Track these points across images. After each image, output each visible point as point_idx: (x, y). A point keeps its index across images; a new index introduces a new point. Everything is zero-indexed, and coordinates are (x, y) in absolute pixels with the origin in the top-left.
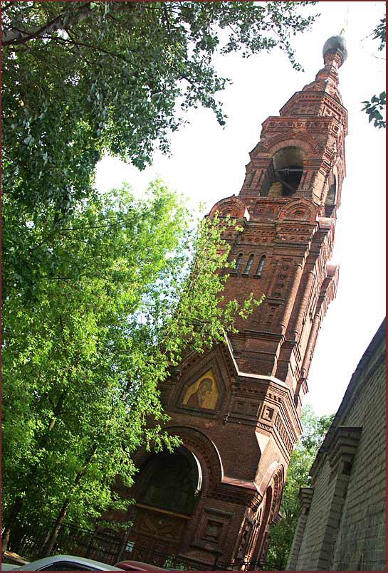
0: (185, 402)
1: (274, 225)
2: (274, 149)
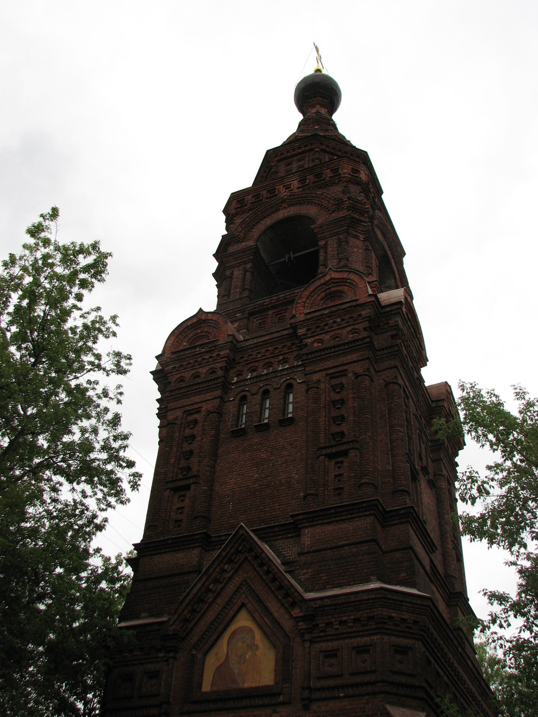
0: (206, 687)
1: (291, 331)
2: (256, 232)
